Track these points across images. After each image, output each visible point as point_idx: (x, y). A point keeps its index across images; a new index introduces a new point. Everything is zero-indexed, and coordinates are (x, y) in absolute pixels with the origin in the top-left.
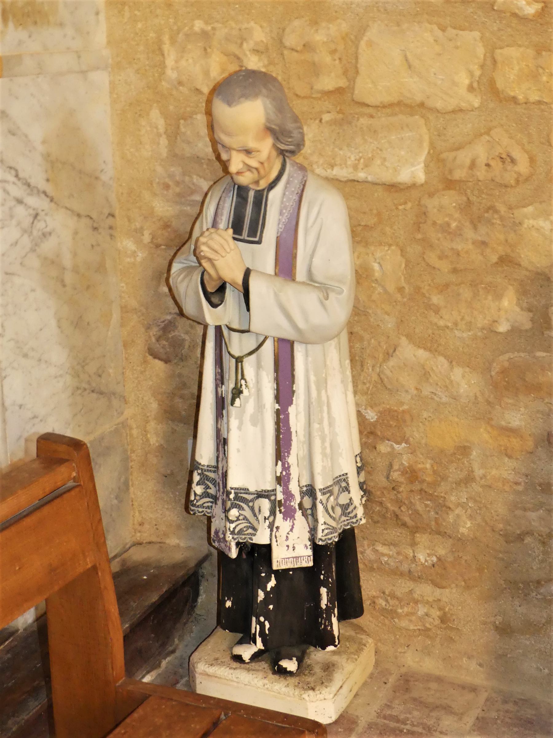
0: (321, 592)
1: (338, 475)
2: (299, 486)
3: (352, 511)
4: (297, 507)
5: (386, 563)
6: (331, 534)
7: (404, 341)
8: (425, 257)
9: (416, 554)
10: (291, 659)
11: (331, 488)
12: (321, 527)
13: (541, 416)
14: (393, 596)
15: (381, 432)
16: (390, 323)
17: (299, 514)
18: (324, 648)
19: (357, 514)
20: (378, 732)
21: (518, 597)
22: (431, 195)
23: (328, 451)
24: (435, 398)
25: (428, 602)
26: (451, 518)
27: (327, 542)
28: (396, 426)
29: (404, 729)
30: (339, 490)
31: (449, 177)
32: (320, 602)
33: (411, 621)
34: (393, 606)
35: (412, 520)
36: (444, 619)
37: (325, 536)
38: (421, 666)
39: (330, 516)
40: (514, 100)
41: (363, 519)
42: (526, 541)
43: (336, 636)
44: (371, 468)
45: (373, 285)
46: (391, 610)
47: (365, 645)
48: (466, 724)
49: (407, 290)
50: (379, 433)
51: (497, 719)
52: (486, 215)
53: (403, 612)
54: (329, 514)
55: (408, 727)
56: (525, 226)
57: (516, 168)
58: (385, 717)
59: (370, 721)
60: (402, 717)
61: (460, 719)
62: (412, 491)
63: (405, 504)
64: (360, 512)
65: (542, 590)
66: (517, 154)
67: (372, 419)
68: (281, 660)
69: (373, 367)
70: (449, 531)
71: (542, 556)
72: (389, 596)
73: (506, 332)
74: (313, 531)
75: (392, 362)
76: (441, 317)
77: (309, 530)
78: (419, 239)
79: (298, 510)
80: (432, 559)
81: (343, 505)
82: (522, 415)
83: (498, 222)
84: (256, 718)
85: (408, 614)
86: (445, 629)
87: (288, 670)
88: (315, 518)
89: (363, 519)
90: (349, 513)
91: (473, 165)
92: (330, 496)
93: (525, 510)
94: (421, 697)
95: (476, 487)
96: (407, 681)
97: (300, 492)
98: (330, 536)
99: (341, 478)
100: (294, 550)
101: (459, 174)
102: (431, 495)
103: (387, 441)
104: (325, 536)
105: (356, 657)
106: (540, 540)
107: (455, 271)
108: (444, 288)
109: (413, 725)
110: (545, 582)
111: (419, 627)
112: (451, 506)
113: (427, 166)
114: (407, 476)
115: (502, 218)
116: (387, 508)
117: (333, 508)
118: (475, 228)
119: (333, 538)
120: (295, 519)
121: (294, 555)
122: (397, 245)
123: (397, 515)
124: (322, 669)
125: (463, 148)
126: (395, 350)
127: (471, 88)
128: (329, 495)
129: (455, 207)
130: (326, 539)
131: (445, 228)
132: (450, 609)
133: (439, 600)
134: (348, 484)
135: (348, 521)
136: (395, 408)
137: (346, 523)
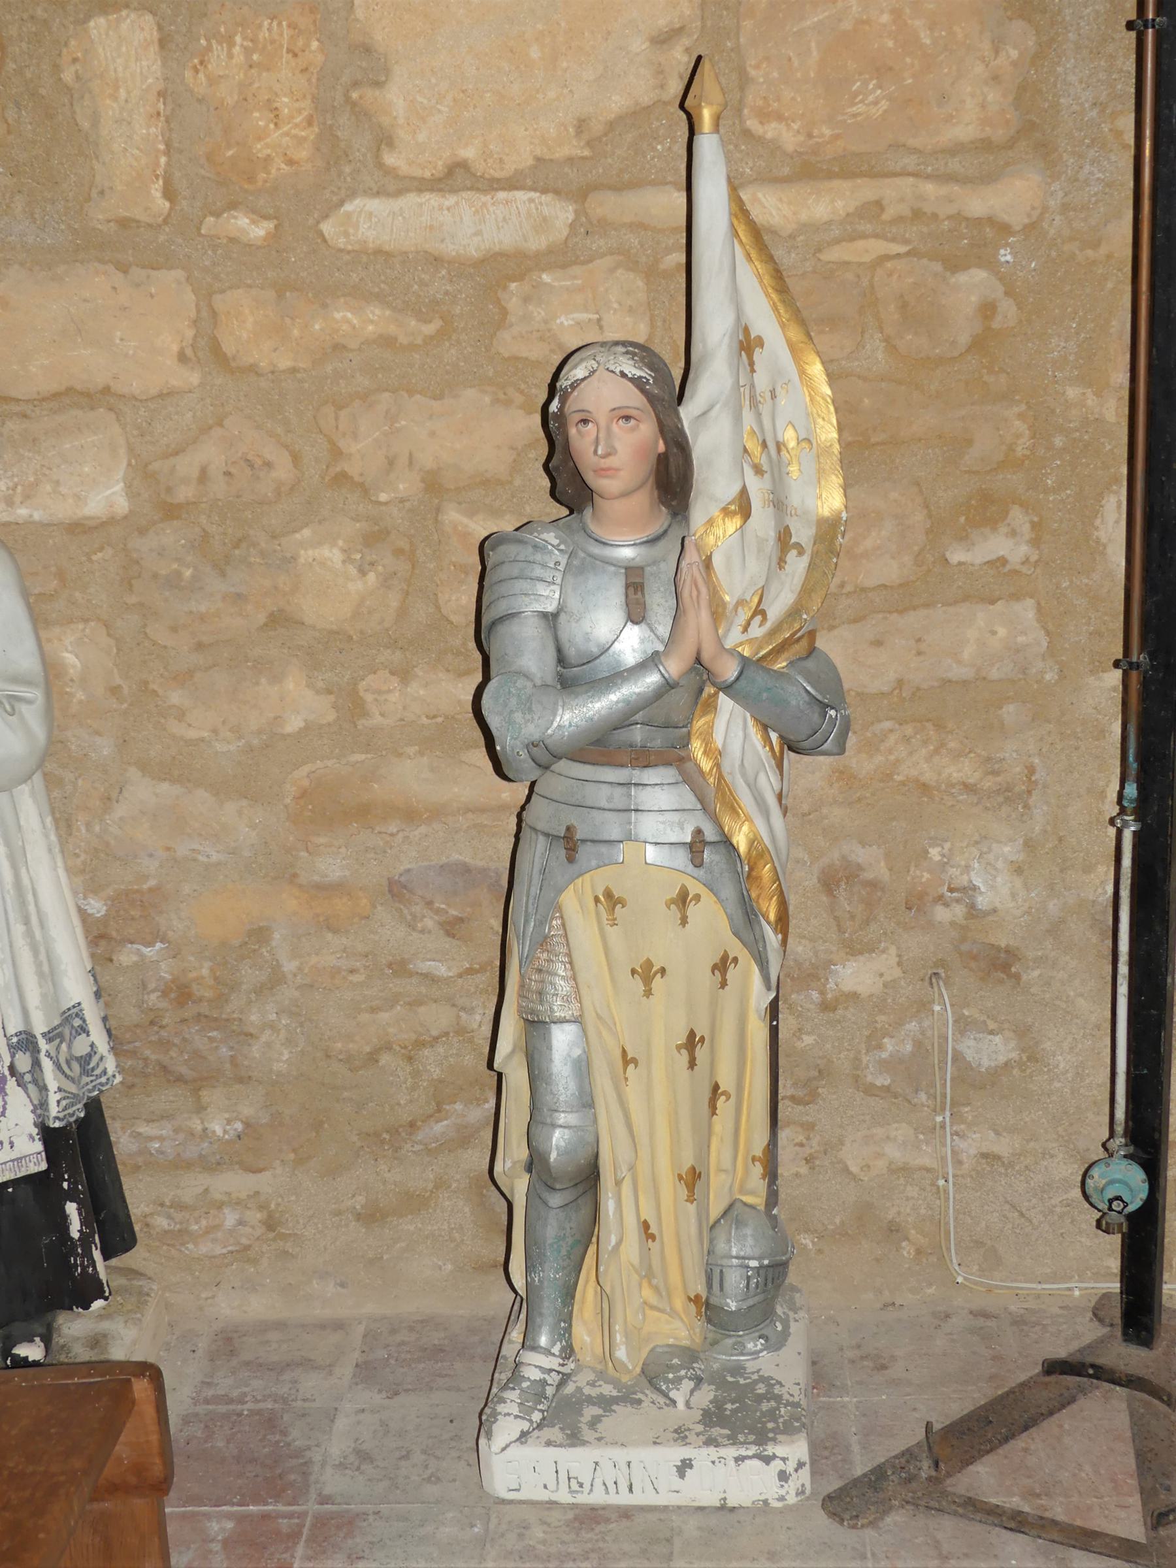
0: (68, 1212)
1: (65, 1008)
2: (5, 1036)
3: (98, 1065)
4: (7, 1073)
5: (160, 1151)
6: (73, 1106)
7: (133, 773)
8: (148, 631)
9: (207, 1125)
10: (33, 1341)
11: (60, 1030)
12: (53, 1098)
13: (372, 855)
14: (179, 1206)
15: (117, 931)
16: (105, 748)
17: (11, 1083)
18: (86, 1307)
19: (106, 1069)
20: (202, 1425)
21: (384, 1156)
22: (142, 532)
23: (46, 968)
24: (200, 858)
25: (238, 1203)
26: (256, 1051)
27: (68, 1121)
28: (141, 916)
29: (243, 1410)
30: (71, 1034)
31: (169, 500)
32: (68, 1228)
33: (214, 1241)
34: (181, 1223)
35: (191, 1069)
36: (271, 1224)
37: (63, 1110)
38: (245, 1312)
39: (66, 1076)
40: (253, 369)
41: (117, 1075)
42: (382, 1062)
43: (105, 1282)
44: (109, 995)
45: (68, 690)
46: (180, 1231)
47: (148, 1295)
48: (340, 1378)
49: (126, 690)
50: (114, 934)
51: (388, 1359)
52: (237, 552)
53: (200, 1228)
54: (63, 1073)
55: (250, 1405)
56: (302, 560)
57: (274, 474)
58: (207, 1401)
59: (185, 1413)
60: (235, 1394)
61: (330, 1373)
62: (184, 1021)
63: (175, 1045)
64: (110, 1064)
65: (420, 1136)
66: (270, 451)
67: (98, 912)
68: (15, 1346)
69: (88, 825)
70: (256, 1073)
71: (410, 1080)
72: (171, 1207)
73: (298, 732)
74: (41, 1106)
75: (120, 811)
76: (190, 725)
77: (32, 1108)
78: (133, 605)
79: (9, 1077)
80: (236, 1126)
81: (81, 1057)
82: (344, 859)
83: (258, 560)
84: (44, 1382)
85: (208, 1231)
86: (274, 1240)
87: (30, 1359)
88: (41, 1084)
89: (117, 1075)
90: (93, 1069)
91: (203, 476)
92: (61, 1042)
93: (374, 1010)
94: (257, 1358)
95: (287, 994)
96: (229, 1340)
97: (8, 1045)
98: (70, 1111)
99: (70, 1012)
100: (12, 1147)
101: (184, 493)
102: (216, 1020)
103: (130, 945)
104: (63, 1110)
105: (139, 1316)
106: (403, 1055)
107: (200, 647)
108: (183, 678)
109: (257, 1401)
110: (423, 1121)
111: (230, 1248)
112: (252, 1031)
113: (128, 486)
114: (173, 995)
115: (262, 554)
116: (146, 1059)
117: (68, 1062)
118: (223, 574)
119: (77, 1113)
120: (6, 1094)
121: (14, 1155)
122: (99, 619)
123: (165, 1067)
124: (87, 1346)
125: (184, 451)
126: (121, 792)
127: (182, 358)
128: (58, 1040)
129: (183, 546)
130: (65, 1116)
131: (173, 582)
132: (278, 1205)
133: (257, 1193)
134: (84, 1021)
135: (94, 1084)
136: (136, 887)
137: (90, 1087)
